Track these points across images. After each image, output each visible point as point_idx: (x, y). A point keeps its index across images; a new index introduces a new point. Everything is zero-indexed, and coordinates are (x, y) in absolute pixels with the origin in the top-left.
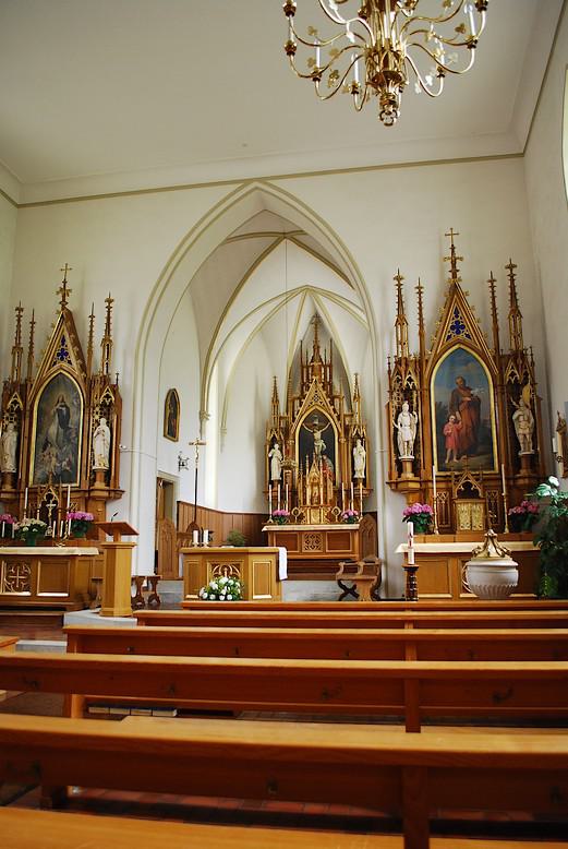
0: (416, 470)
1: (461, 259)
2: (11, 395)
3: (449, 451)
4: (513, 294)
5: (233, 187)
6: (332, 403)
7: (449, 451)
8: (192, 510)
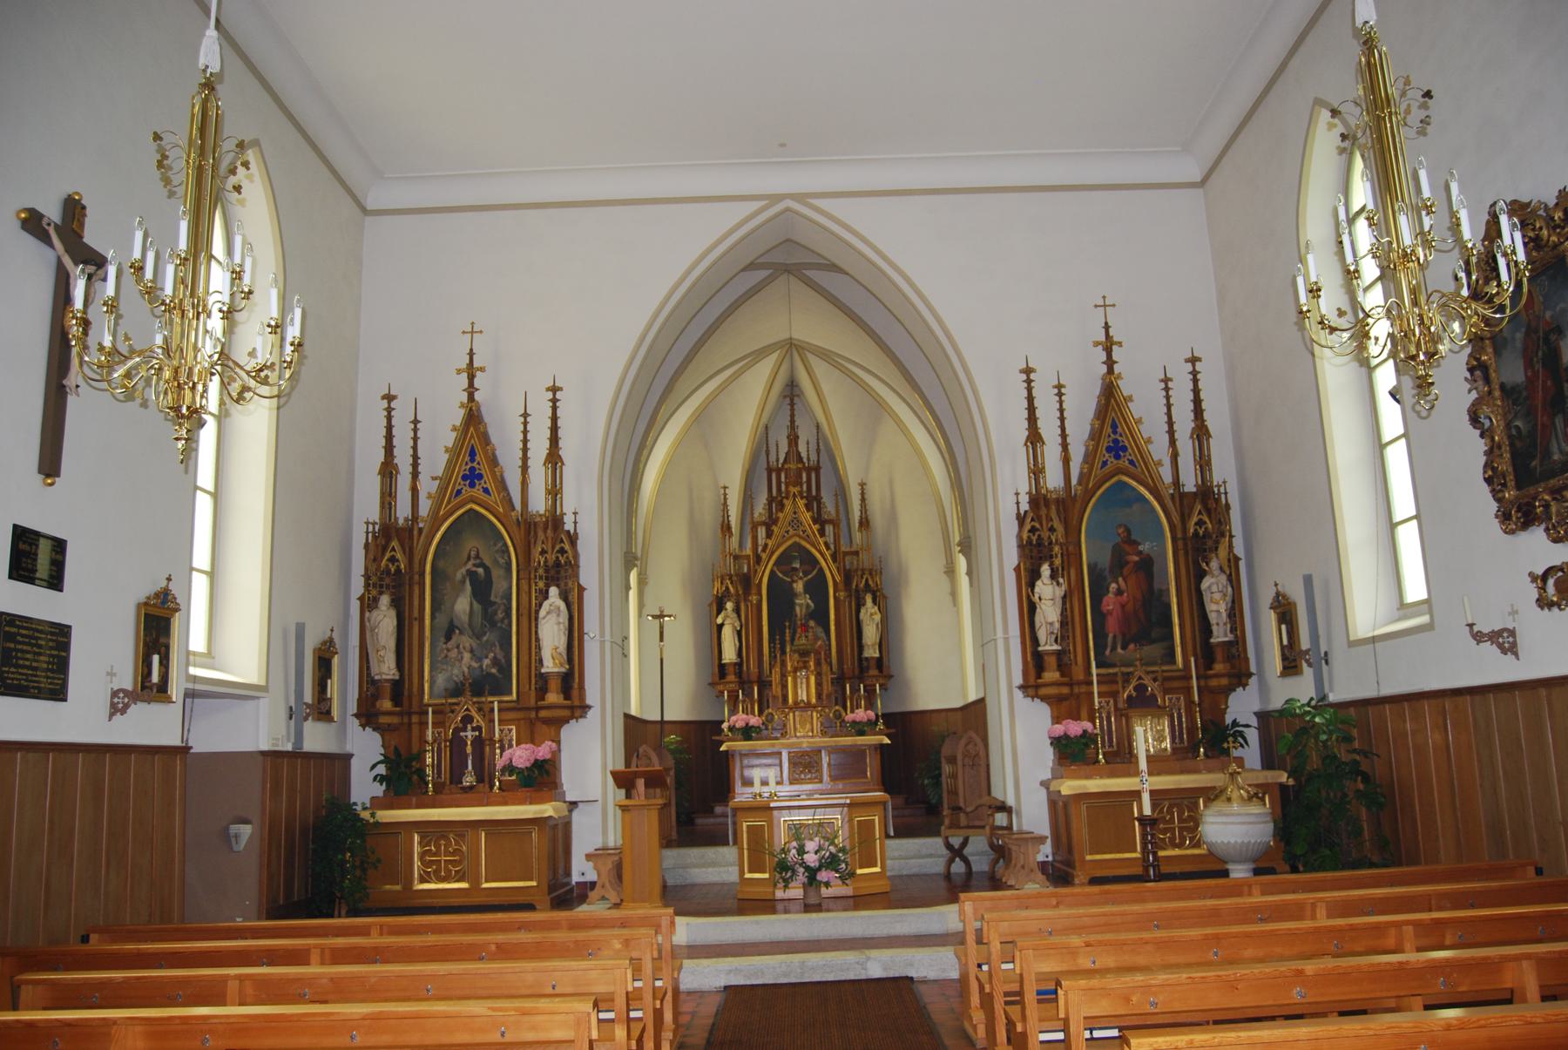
0: (1063, 667)
1: (1120, 344)
2: (384, 549)
4: (1197, 401)
5: (756, 205)
6: (822, 533)
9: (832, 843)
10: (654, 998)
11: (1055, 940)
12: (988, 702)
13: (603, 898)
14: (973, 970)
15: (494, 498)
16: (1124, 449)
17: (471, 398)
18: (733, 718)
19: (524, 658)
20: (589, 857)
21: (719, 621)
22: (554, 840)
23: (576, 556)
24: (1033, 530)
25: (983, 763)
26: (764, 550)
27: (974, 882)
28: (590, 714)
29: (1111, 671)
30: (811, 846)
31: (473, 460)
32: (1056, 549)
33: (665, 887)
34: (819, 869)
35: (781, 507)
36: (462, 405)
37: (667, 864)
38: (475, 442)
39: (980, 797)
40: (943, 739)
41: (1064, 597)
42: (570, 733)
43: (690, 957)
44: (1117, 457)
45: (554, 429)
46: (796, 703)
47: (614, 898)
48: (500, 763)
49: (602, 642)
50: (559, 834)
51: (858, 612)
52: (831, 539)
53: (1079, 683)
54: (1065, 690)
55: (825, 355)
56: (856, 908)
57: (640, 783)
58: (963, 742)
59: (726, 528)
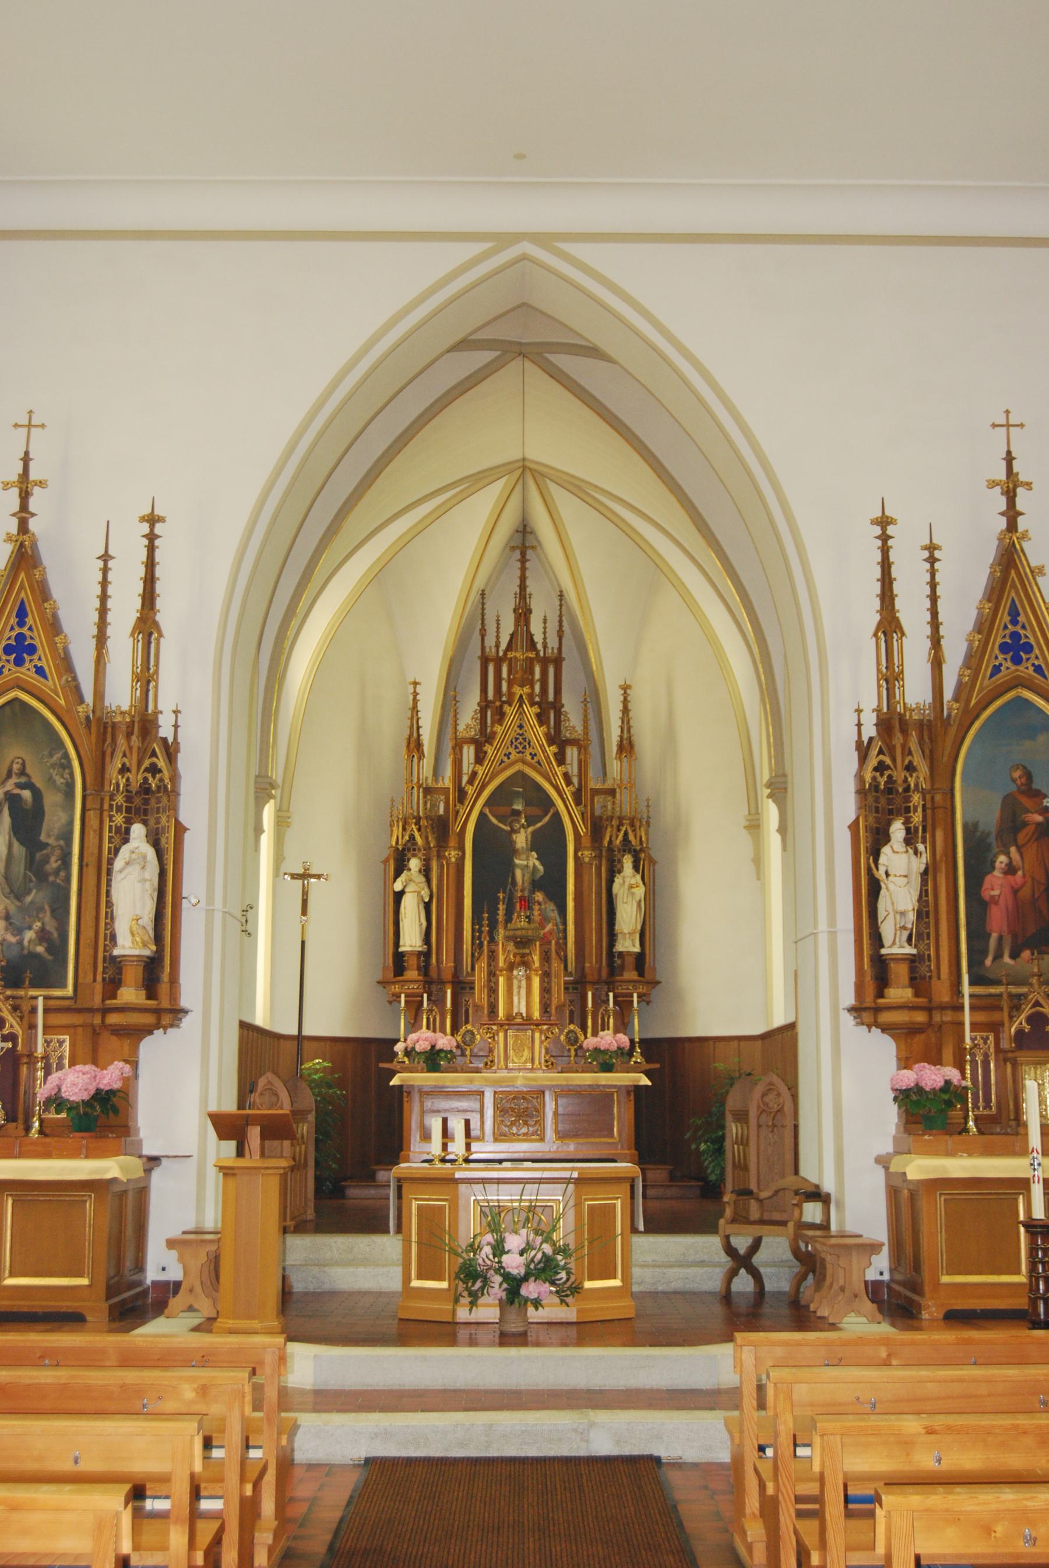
0: (918, 982)
3: (994, 936)
6: (561, 759)
7: (994, 936)
8: (292, 1046)
9: (547, 1239)
10: (243, 1479)
11: (874, 1421)
12: (801, 1029)
13: (191, 1309)
14: (750, 1454)
15: (53, 684)
16: (1028, 648)
17: (23, 527)
18: (413, 1037)
19: (88, 933)
20: (171, 1244)
21: (398, 886)
22: (119, 1216)
23: (175, 777)
24: (880, 768)
25: (789, 1123)
26: (471, 782)
27: (766, 1309)
28: (186, 1021)
29: (993, 990)
30: (514, 1242)
31: (21, 623)
32: (916, 798)
33: (286, 1294)
34: (525, 1278)
35: (500, 716)
36: (9, 538)
37: (292, 1259)
38: (27, 595)
39: (783, 1176)
40: (732, 1081)
41: (925, 874)
42: (151, 1048)
43: (317, 1409)
44: (1017, 660)
45: (150, 580)
46: (510, 1017)
47: (206, 1308)
48: (42, 1092)
49: (210, 913)
50: (128, 1207)
51: (610, 882)
52: (573, 770)
53: (942, 1008)
54: (920, 1017)
55: (578, 488)
56: (581, 1341)
57: (254, 1134)
58: (759, 1090)
59: (414, 745)
